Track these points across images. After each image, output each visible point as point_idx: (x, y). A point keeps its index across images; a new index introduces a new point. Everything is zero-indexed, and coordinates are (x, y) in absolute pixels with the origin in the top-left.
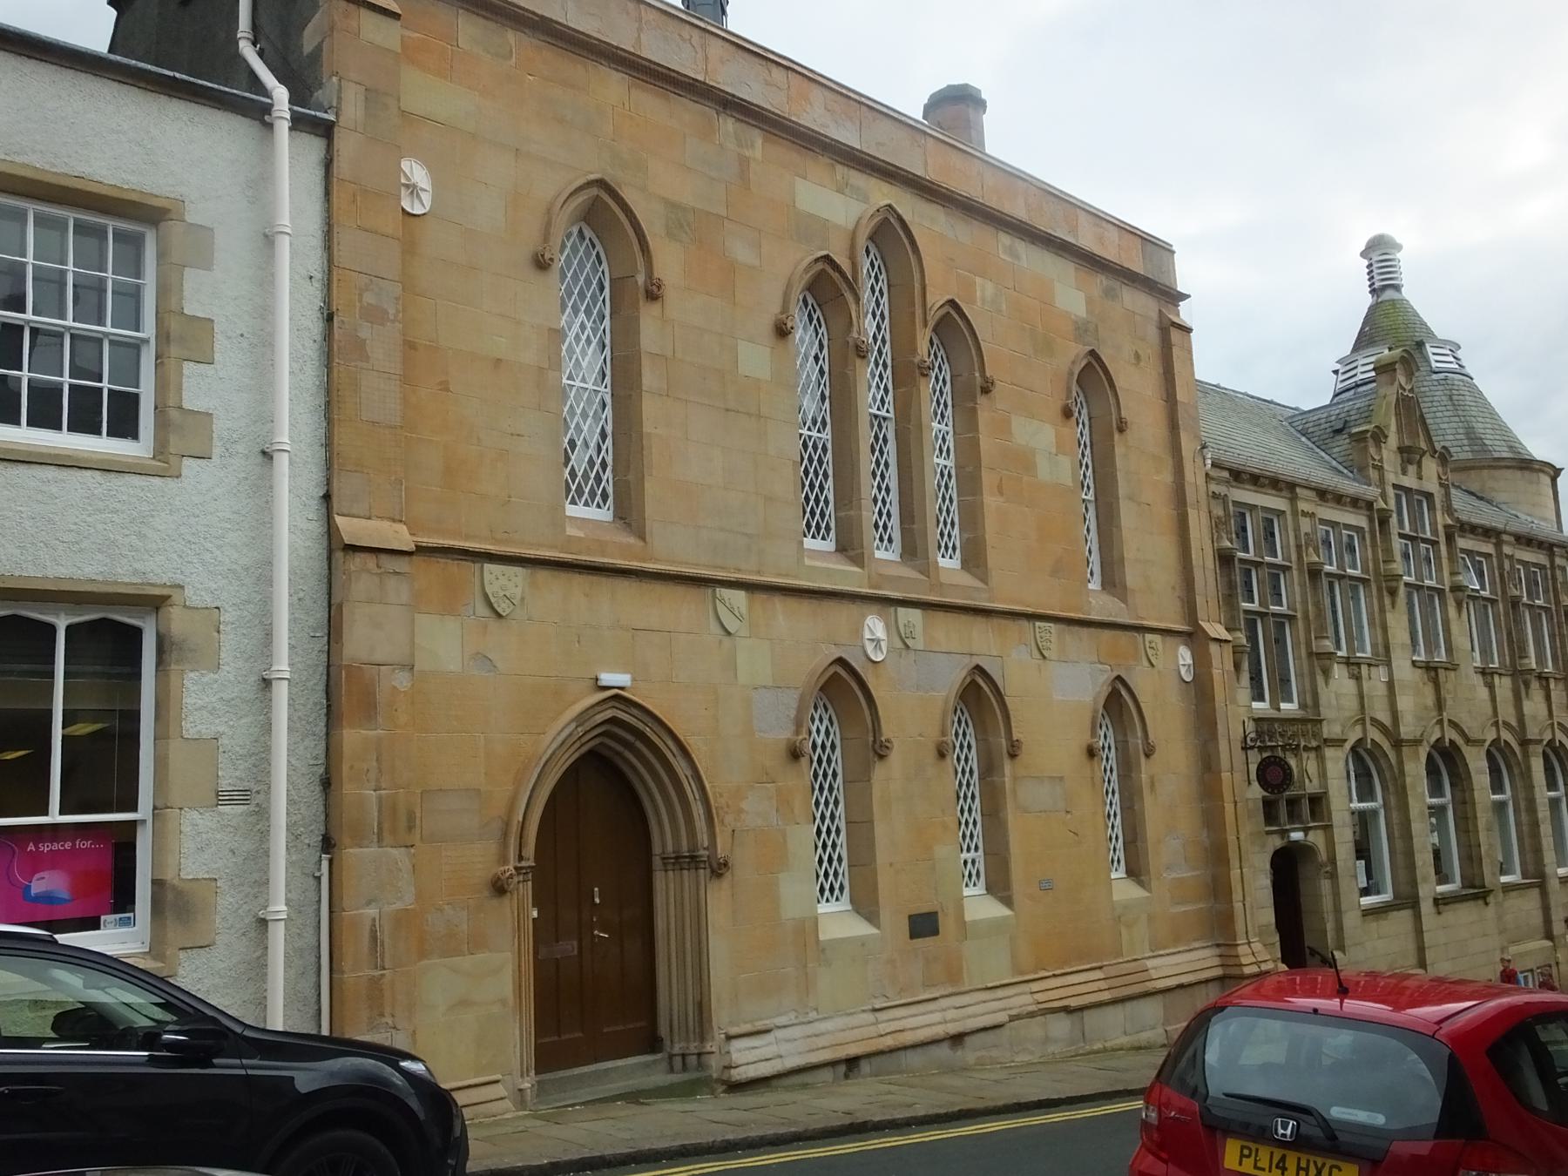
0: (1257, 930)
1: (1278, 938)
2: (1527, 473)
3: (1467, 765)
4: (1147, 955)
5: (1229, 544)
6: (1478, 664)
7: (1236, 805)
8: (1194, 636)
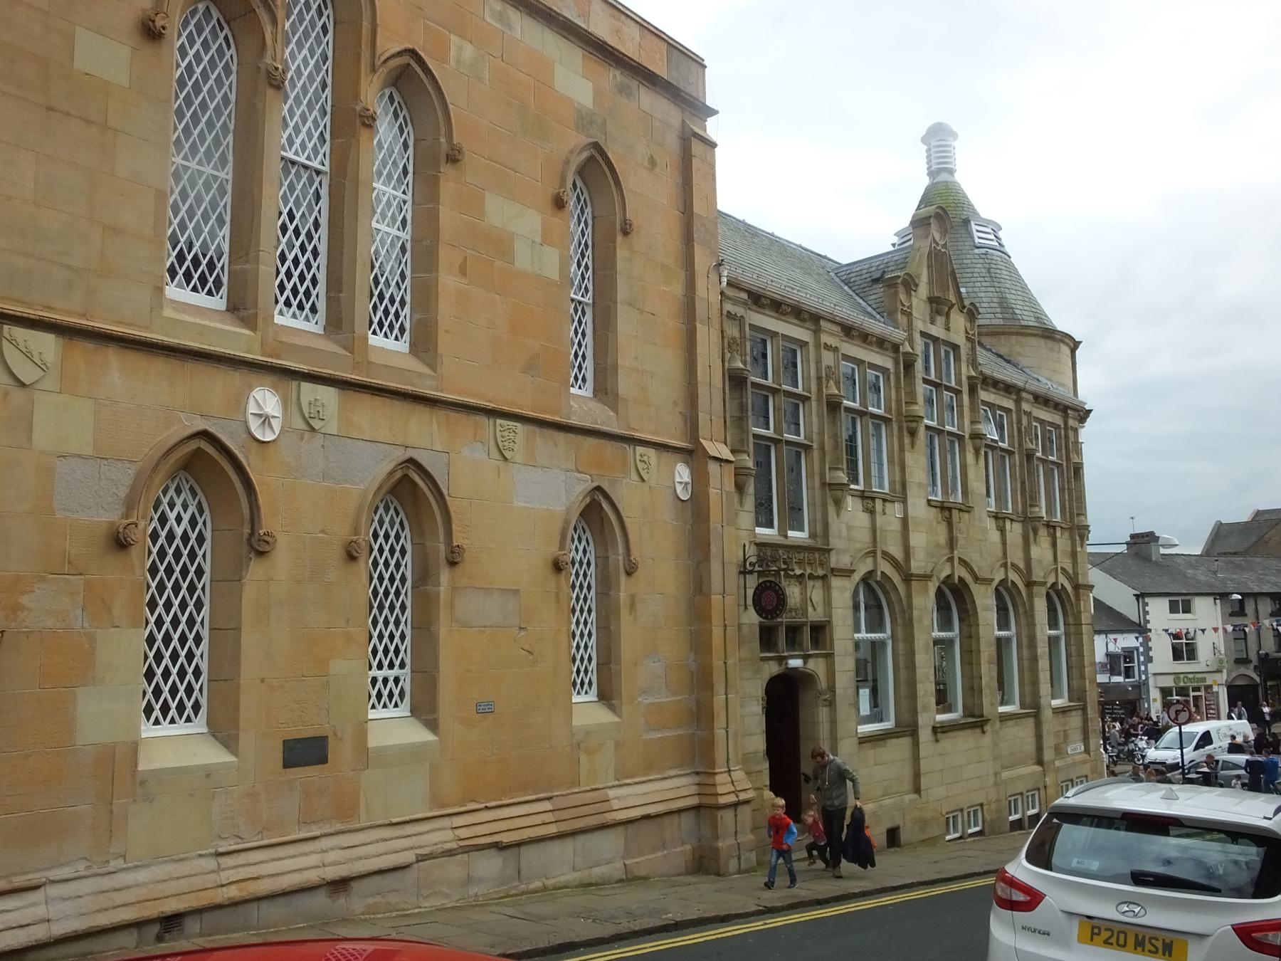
0: (740, 757)
1: (767, 765)
2: (1050, 343)
3: (974, 602)
4: (610, 784)
5: (741, 366)
6: (993, 509)
7: (725, 629)
8: (693, 454)
